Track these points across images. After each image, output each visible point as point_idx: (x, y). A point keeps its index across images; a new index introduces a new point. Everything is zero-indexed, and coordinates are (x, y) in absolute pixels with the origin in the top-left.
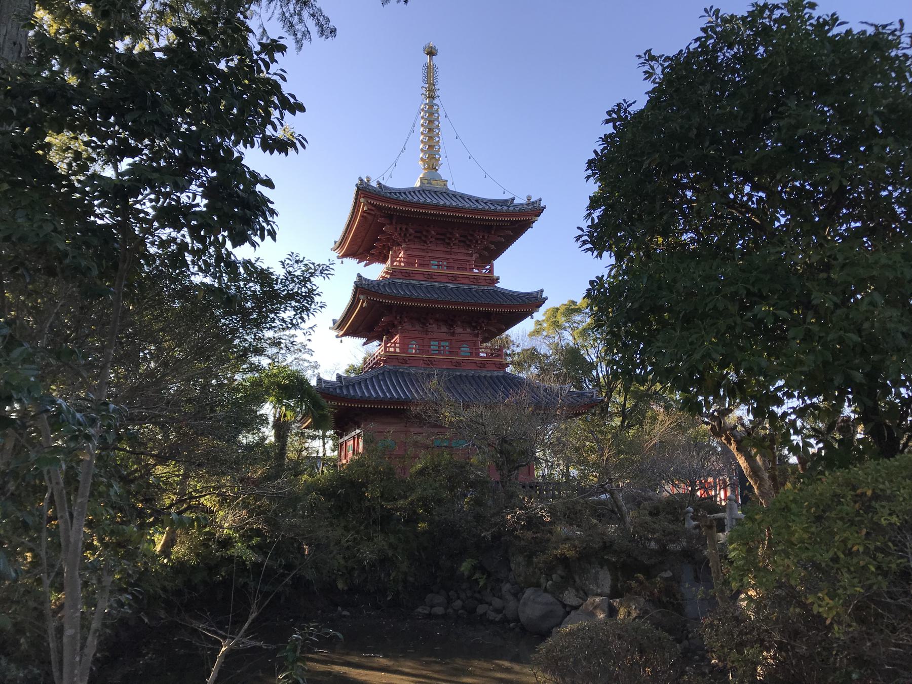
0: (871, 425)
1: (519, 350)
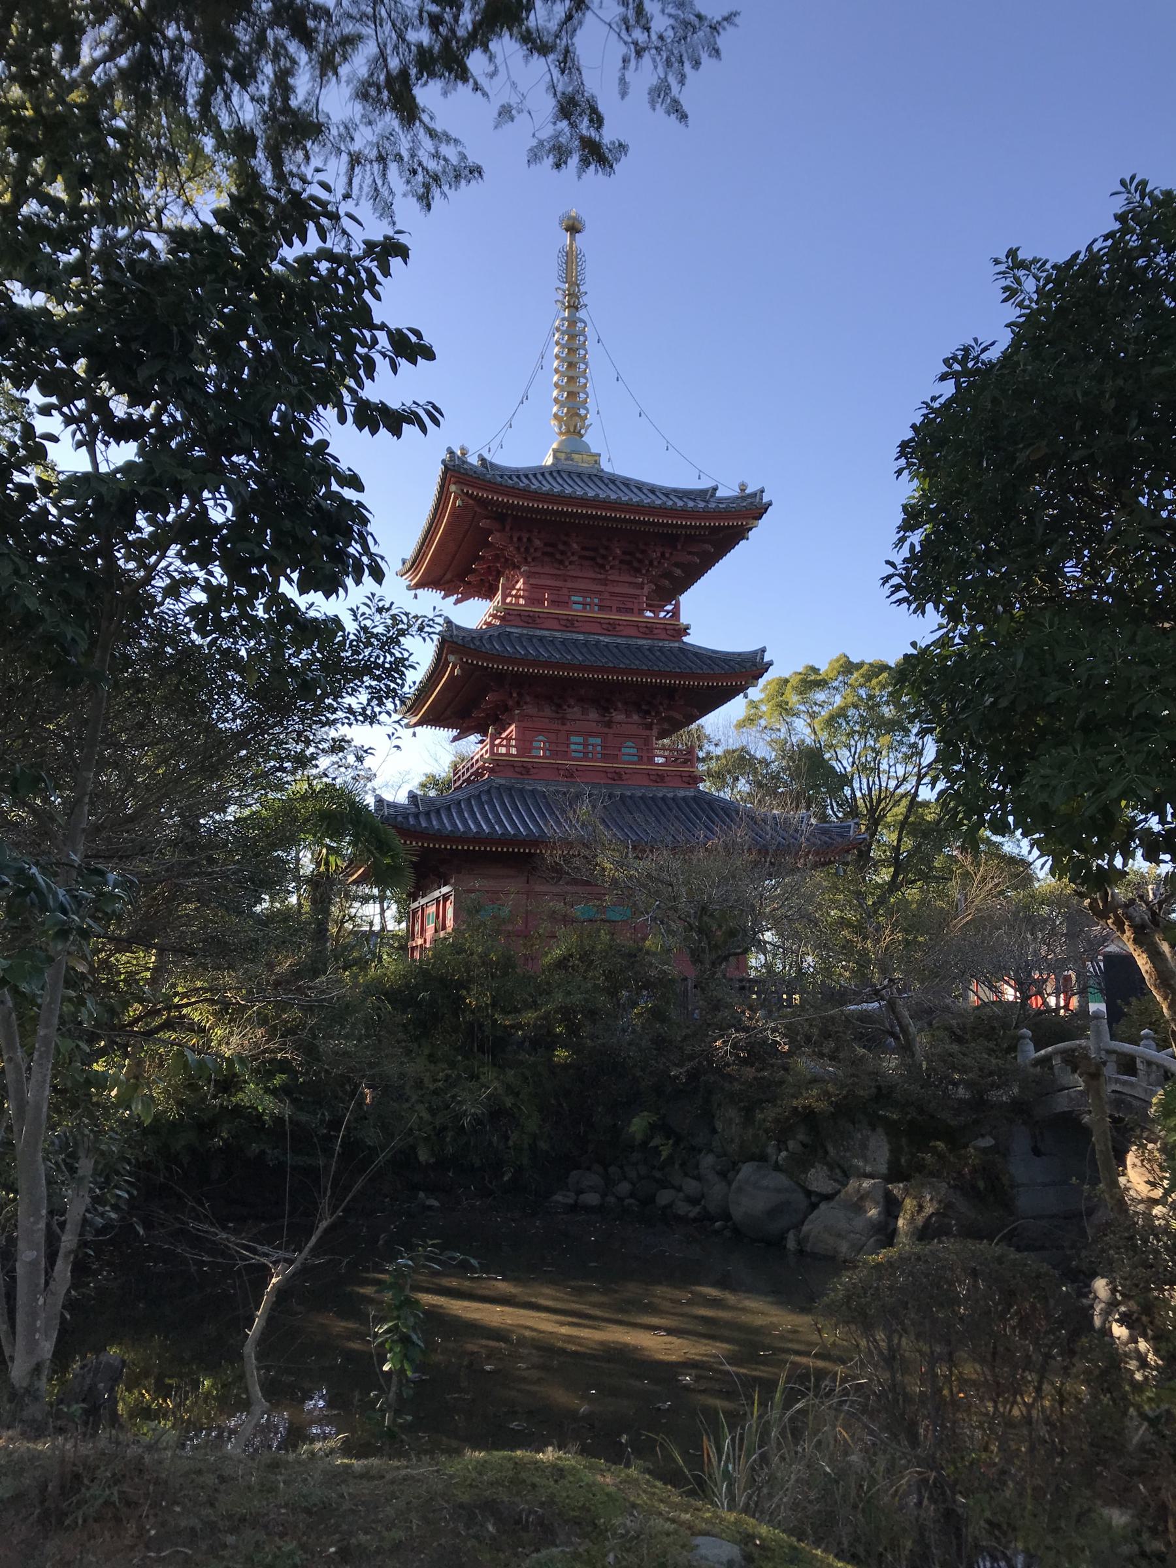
1: (719, 751)
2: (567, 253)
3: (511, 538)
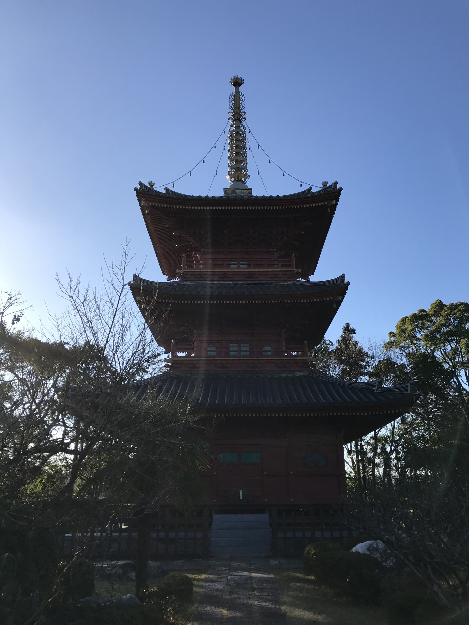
2: (234, 96)
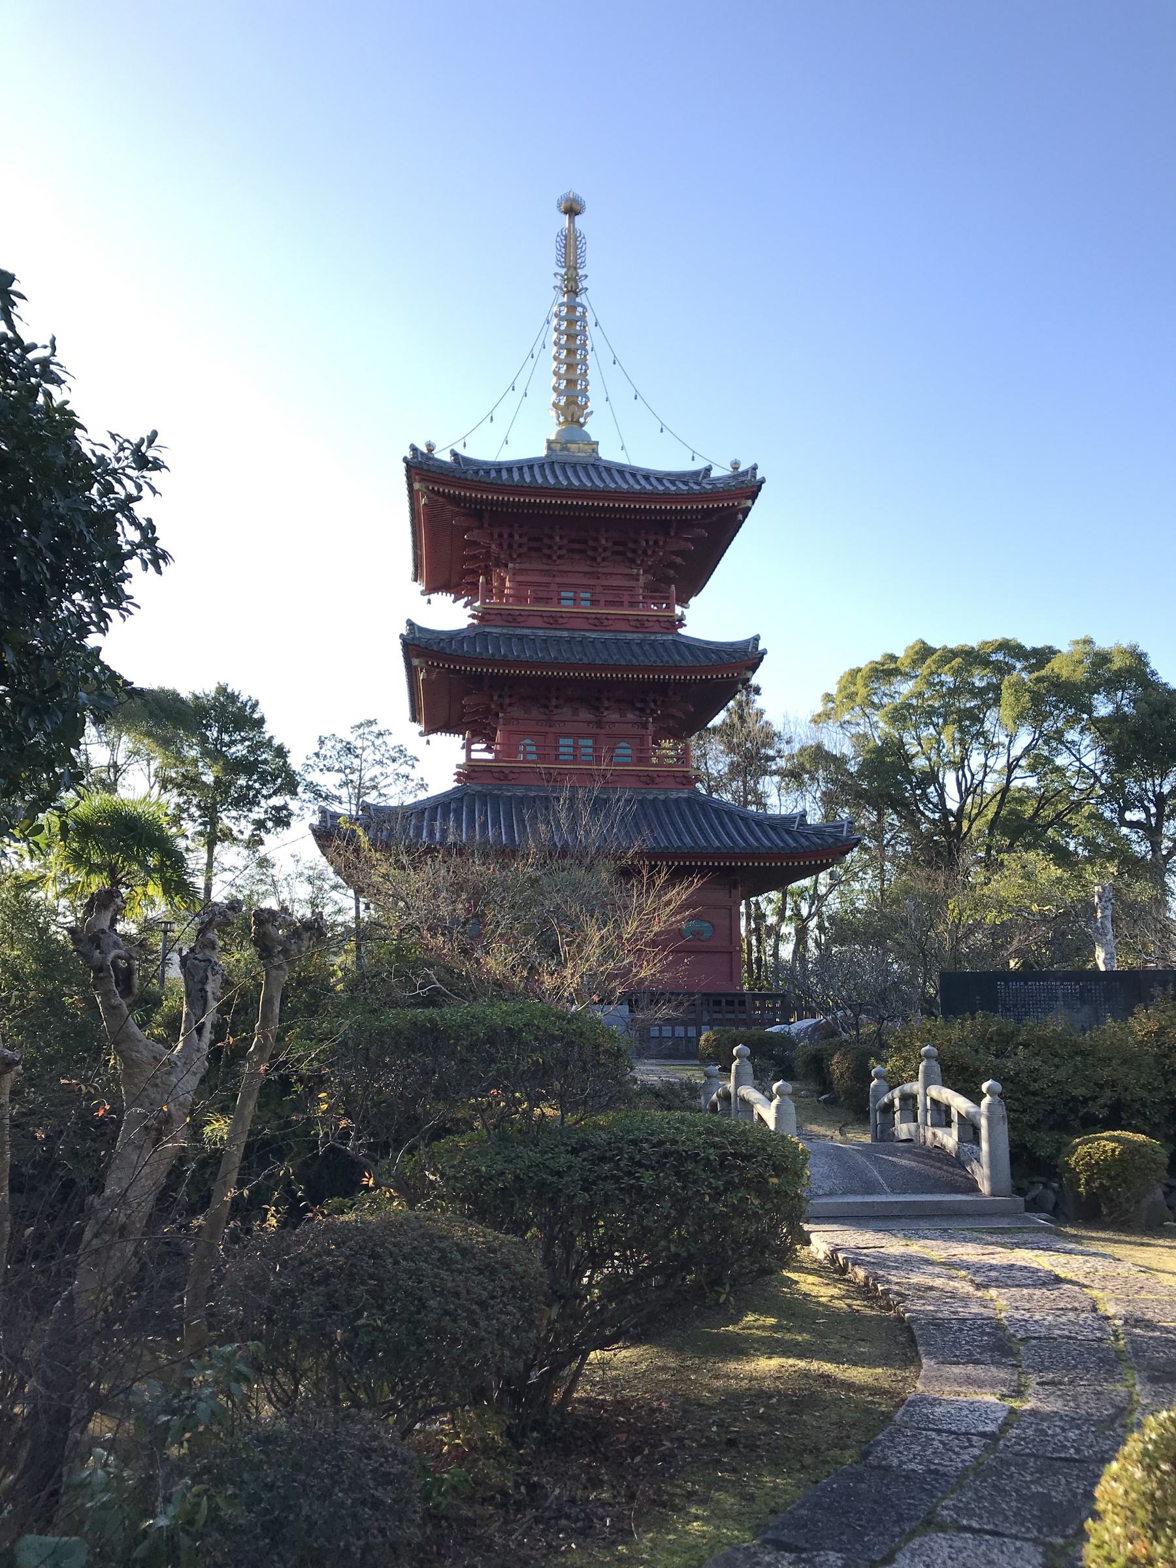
0: (174, 1107)
1: (787, 750)
2: (566, 236)
3: (492, 534)
